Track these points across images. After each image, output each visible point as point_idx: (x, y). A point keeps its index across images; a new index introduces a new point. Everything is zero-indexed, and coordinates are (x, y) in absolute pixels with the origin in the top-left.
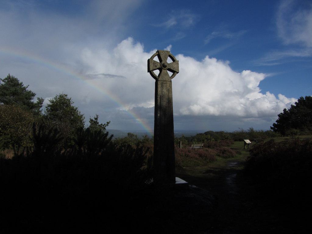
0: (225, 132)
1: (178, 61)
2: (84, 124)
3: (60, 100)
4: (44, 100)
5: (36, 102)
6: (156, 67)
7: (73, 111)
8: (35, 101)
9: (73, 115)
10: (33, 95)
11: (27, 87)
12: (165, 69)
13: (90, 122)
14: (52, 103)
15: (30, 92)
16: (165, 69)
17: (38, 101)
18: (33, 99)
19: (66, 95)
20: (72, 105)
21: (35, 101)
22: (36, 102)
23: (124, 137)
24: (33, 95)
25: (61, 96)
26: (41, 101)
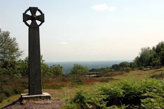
1: (44, 14)
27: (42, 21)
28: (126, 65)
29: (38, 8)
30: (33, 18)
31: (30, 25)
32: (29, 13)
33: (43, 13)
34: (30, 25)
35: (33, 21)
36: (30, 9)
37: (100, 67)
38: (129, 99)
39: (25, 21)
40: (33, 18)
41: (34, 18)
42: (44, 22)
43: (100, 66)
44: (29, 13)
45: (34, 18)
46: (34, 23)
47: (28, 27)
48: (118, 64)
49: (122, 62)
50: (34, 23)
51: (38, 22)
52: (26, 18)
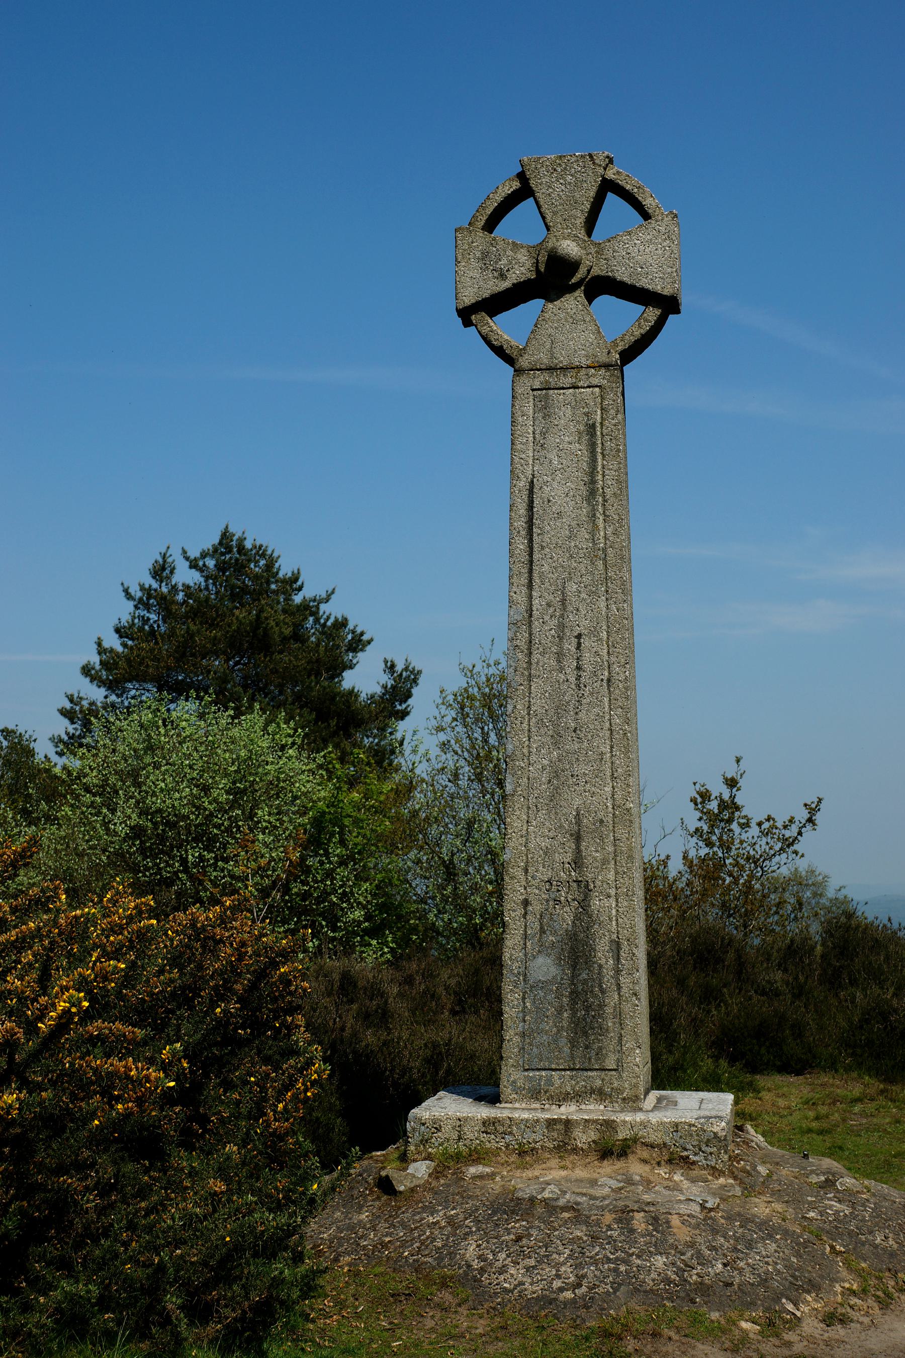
6: (502, 276)
10: (358, 643)
11: (327, 600)
15: (341, 624)
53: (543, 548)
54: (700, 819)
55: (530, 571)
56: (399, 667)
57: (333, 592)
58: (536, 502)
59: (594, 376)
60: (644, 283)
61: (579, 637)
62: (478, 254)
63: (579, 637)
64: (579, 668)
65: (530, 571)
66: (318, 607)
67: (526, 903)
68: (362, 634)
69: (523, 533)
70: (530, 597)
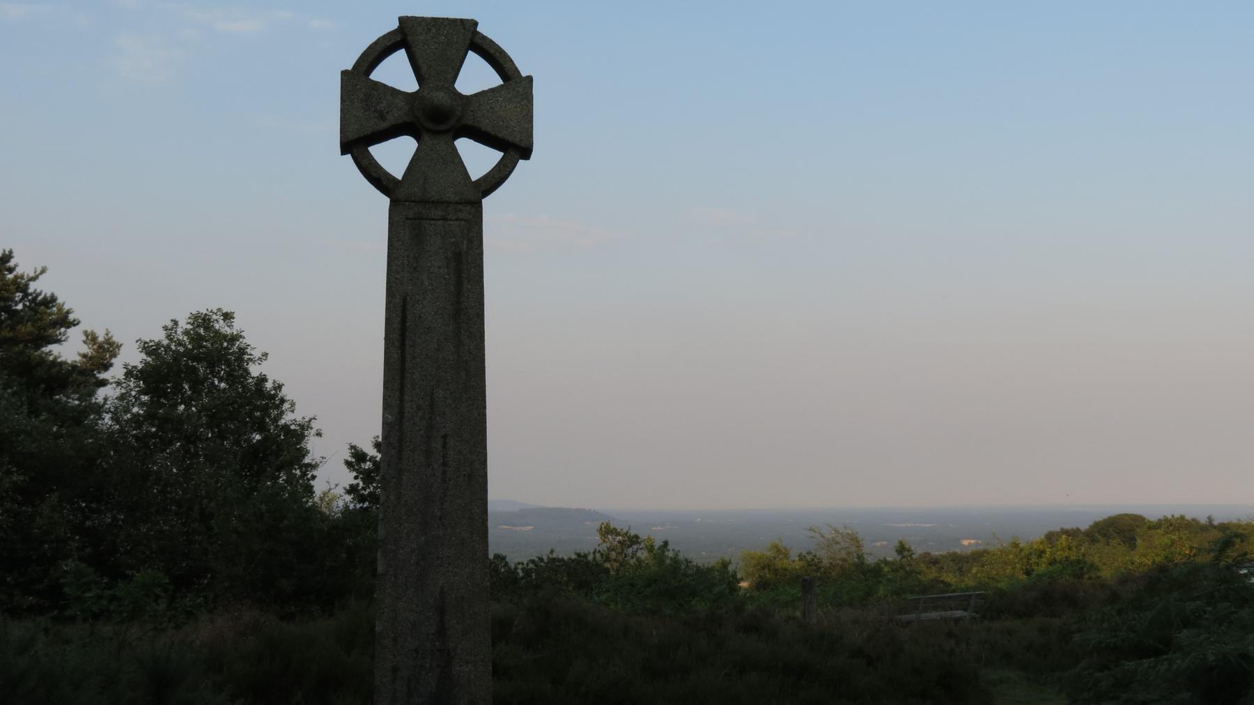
0: (1216, 523)
1: (530, 79)
2: (314, 477)
3: (196, 339)
4: (119, 347)
5: (78, 358)
6: (382, 117)
7: (262, 401)
8: (69, 349)
9: (262, 428)
10: (65, 321)
11: (34, 279)
12: (443, 127)
13: (348, 464)
14: (148, 354)
15: (50, 301)
16: (443, 127)
17: (85, 349)
18: (58, 341)
19: (227, 317)
20: (254, 370)
21: (69, 349)
22: (78, 358)
23: (1037, 535)
24: (65, 321)
25: (202, 321)
26: (103, 352)
27: (516, 148)
28: (33, 287)
29: (344, 73)
30: (437, 118)
31: (400, 177)
32: (397, 73)
33: (524, 74)
34: (400, 177)
35: (426, 138)
36: (407, 36)
37: (1028, 556)
38: (20, 307)
39: (356, 144)
40: (437, 118)
41: (437, 125)
42: (526, 153)
43: (966, 543)
44: (397, 73)
45: (437, 125)
46: (436, 162)
47: (386, 201)
48: (1084, 527)
49: (1106, 517)
50: (436, 162)
51: (477, 158)
52: (366, 116)
53: (414, 358)
54: (356, 478)
55: (402, 378)
56: (101, 339)
57: (43, 271)
58: (409, 317)
59: (460, 211)
60: (502, 134)
61: (445, 437)
62: (361, 96)
63: (445, 437)
64: (444, 464)
65: (402, 378)
66: (27, 286)
67: (395, 670)
68: (68, 312)
69: (397, 344)
70: (402, 400)
